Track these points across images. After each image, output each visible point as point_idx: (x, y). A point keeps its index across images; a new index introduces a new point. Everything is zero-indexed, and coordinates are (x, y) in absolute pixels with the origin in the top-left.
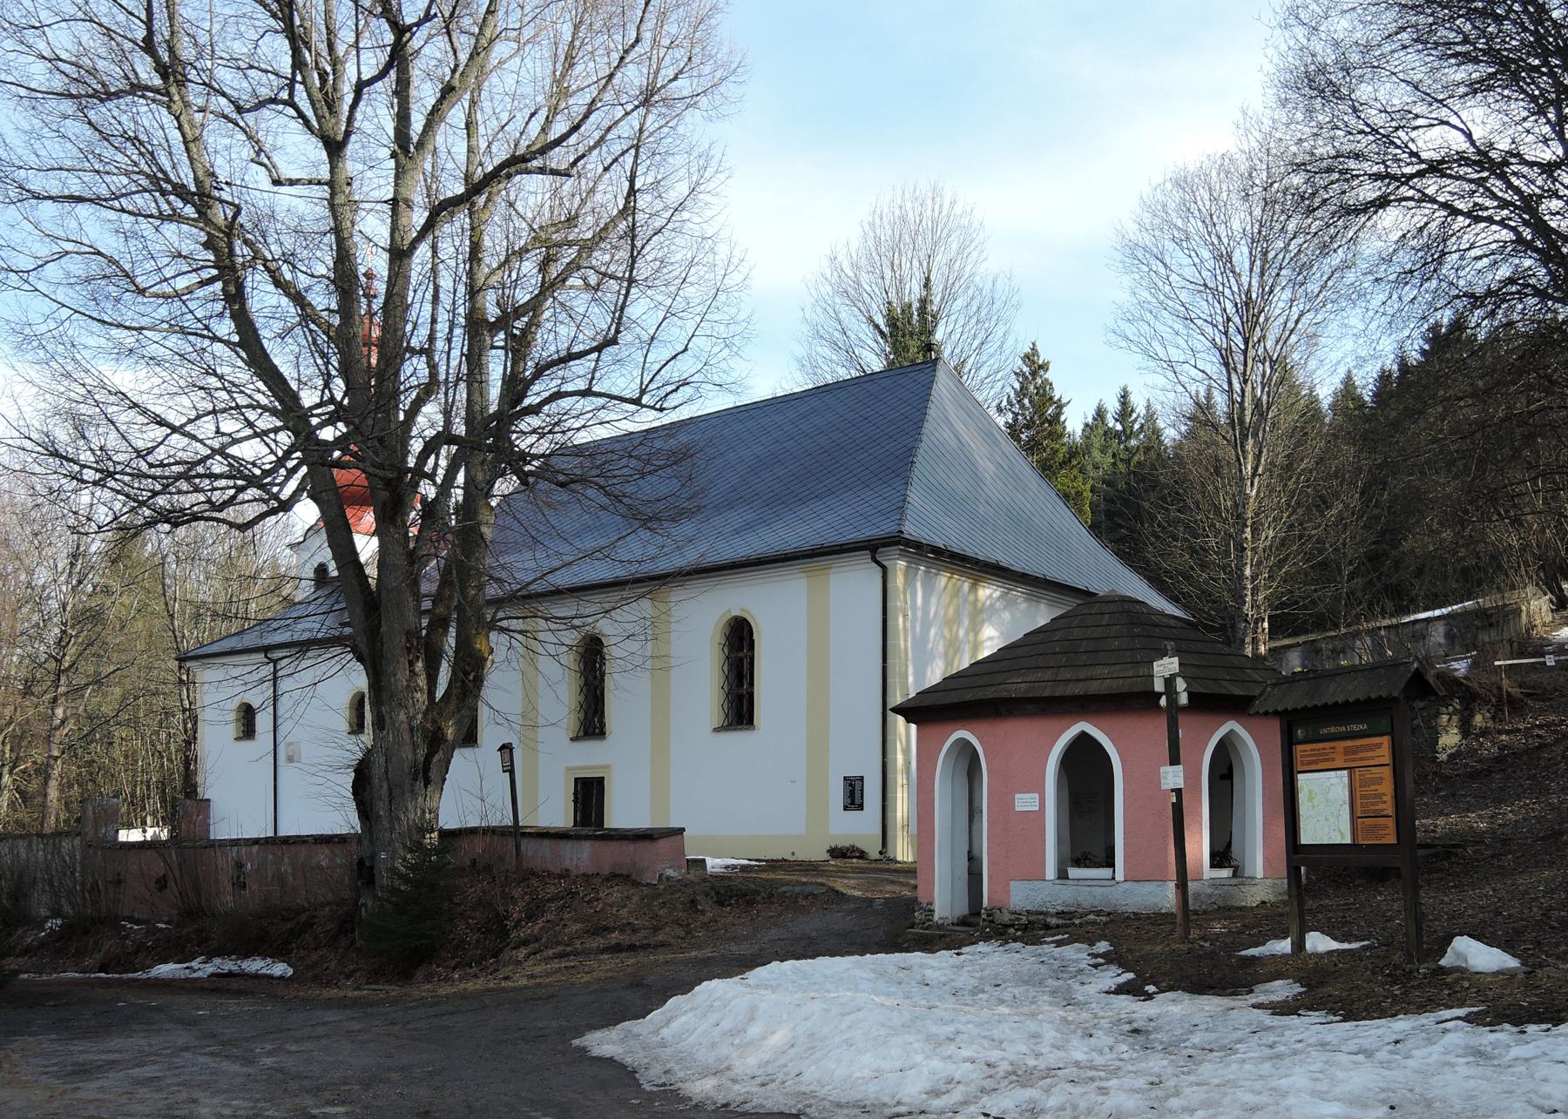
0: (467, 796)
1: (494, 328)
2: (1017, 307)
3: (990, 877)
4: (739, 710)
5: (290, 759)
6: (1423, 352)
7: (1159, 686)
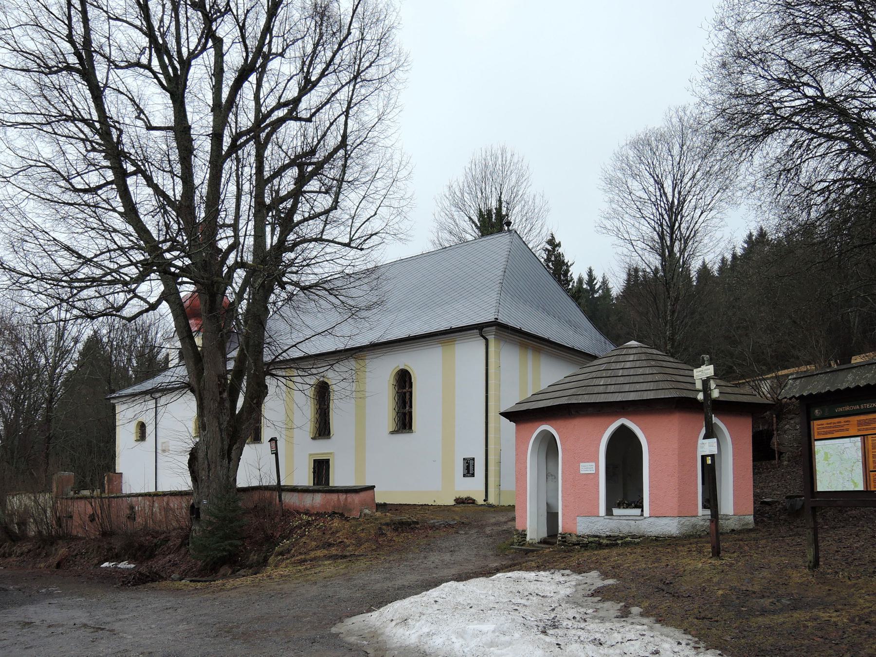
0: (253, 468)
1: (269, 208)
2: (548, 211)
3: (563, 515)
4: (404, 421)
5: (164, 451)
6: (744, 249)
7: (699, 385)
